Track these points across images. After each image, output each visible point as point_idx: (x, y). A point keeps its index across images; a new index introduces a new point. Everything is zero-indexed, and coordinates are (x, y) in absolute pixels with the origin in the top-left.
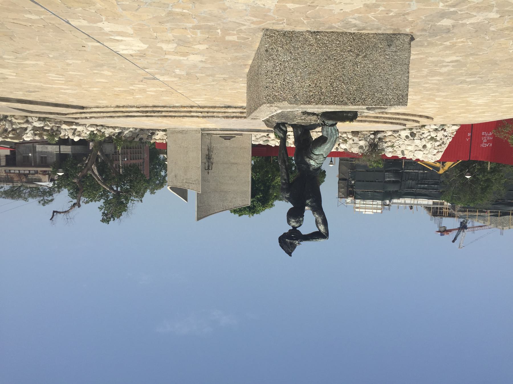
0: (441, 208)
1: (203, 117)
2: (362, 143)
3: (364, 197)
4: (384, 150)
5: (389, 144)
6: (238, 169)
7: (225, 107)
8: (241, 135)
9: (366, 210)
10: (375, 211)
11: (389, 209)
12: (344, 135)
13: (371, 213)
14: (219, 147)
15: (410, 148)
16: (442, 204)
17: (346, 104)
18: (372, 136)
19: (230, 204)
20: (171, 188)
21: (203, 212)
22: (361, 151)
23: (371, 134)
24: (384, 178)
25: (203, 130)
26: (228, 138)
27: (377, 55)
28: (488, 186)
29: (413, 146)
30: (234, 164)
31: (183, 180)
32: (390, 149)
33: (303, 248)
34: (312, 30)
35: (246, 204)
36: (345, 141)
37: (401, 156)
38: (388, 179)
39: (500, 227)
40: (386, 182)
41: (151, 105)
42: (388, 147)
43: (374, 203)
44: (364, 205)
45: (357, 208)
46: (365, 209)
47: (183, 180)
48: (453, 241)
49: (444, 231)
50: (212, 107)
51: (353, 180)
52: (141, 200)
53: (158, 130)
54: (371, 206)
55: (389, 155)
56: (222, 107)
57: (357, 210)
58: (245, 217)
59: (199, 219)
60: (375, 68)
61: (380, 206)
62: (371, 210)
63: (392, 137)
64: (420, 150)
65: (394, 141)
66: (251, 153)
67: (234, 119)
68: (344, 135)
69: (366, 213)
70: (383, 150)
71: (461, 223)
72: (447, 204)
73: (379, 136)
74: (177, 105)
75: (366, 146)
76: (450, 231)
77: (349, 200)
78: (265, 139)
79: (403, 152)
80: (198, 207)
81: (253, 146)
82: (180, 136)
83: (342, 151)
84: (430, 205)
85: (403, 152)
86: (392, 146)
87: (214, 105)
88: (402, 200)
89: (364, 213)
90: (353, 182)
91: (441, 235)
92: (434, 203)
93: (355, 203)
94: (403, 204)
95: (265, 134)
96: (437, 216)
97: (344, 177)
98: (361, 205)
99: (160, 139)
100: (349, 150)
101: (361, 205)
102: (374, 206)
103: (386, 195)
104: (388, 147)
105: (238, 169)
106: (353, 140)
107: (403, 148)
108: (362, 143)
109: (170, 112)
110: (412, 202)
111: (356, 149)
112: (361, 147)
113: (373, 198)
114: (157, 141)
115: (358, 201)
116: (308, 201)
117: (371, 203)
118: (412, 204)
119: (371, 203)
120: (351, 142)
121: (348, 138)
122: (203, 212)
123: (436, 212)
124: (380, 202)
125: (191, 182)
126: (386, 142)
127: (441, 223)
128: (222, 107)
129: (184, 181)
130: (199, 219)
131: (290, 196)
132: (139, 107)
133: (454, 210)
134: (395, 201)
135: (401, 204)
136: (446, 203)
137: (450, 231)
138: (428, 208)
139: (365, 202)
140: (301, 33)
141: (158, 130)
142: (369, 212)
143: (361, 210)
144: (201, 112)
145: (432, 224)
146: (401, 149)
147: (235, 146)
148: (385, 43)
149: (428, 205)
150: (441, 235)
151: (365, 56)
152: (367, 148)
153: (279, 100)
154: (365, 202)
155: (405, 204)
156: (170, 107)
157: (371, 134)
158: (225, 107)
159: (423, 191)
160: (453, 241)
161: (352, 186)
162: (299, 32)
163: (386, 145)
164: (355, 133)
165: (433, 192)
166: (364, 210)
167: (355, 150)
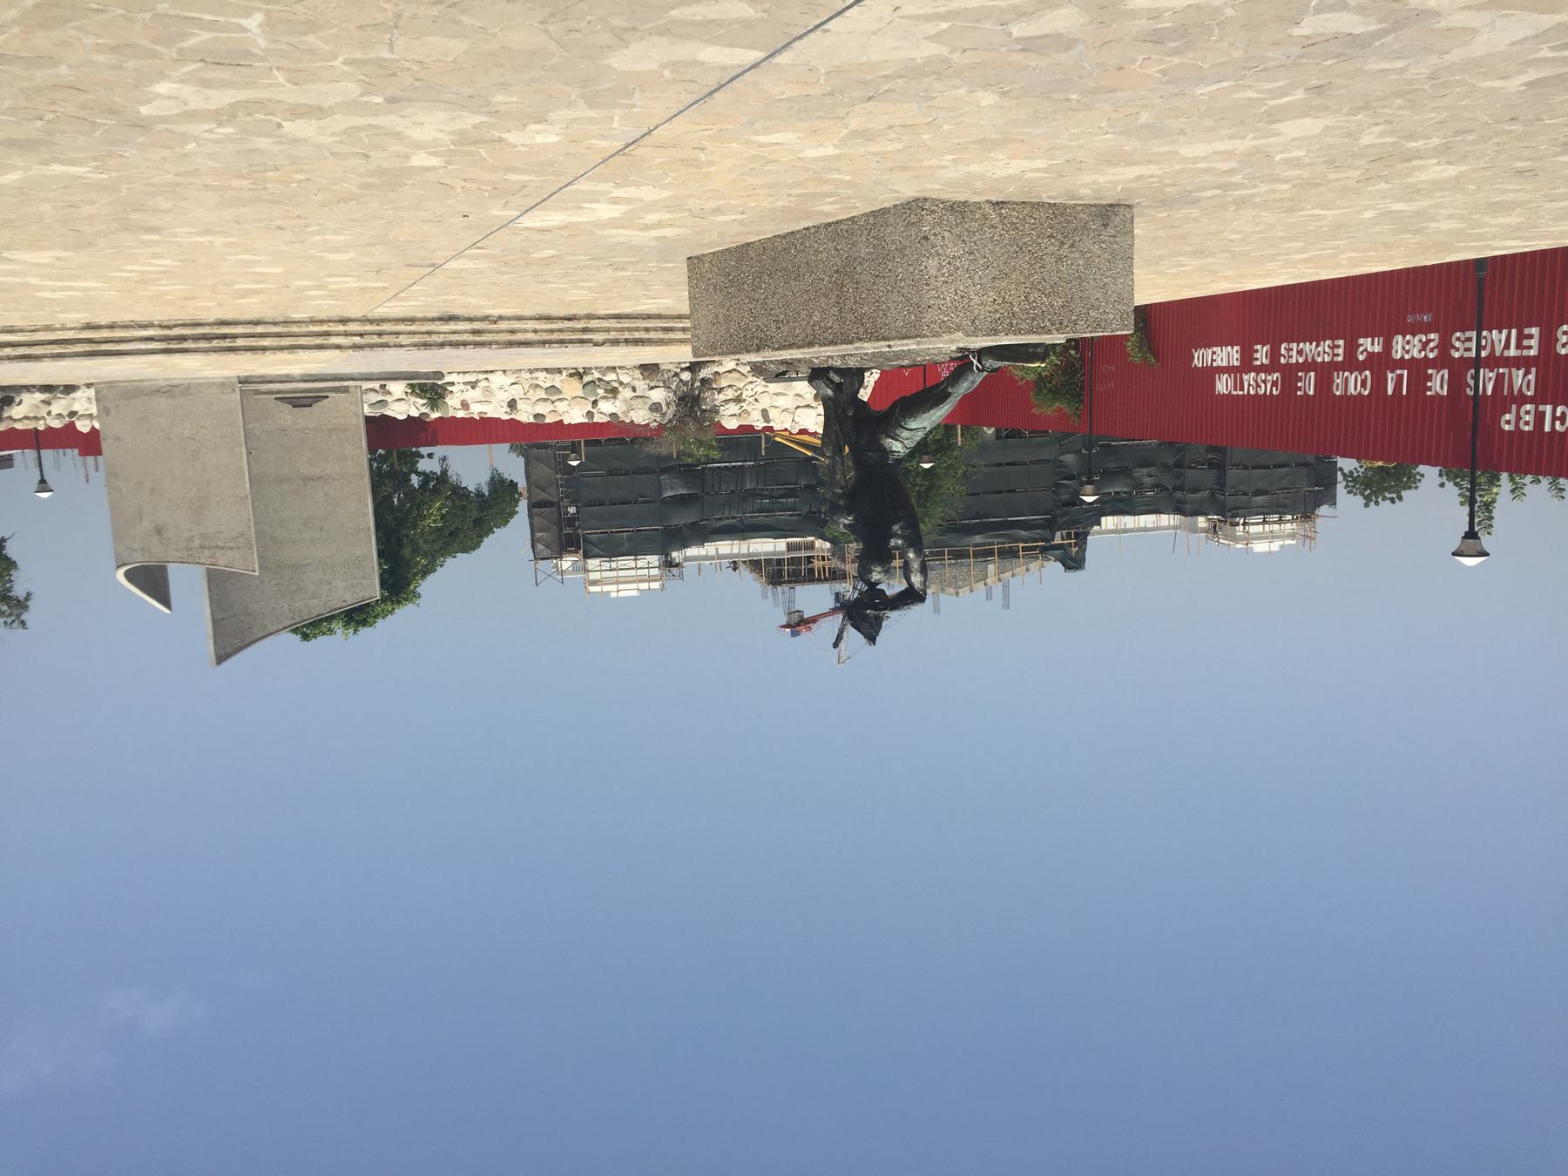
0: (809, 559)
1: (355, 347)
2: (659, 395)
3: (610, 550)
4: (717, 412)
5: (730, 394)
6: (326, 495)
7: (441, 319)
8: (346, 390)
9: (621, 587)
10: (644, 586)
11: (681, 577)
12: (611, 377)
13: (635, 593)
14: (257, 432)
15: (781, 402)
16: (811, 546)
17: (1049, 332)
18: (686, 376)
19: (315, 602)
20: (128, 575)
21: (231, 638)
22: (657, 416)
23: (683, 370)
24: (660, 490)
25: (244, 381)
26: (301, 401)
27: (1088, 243)
28: (930, 488)
29: (790, 397)
30: (307, 479)
31: (190, 539)
32: (733, 408)
33: (896, 623)
34: (994, 199)
35: (367, 595)
36: (613, 392)
37: (759, 424)
38: (669, 493)
39: (951, 590)
40: (664, 501)
41: (211, 320)
42: (727, 401)
43: (640, 563)
44: (614, 574)
45: (595, 583)
46: (617, 583)
47: (190, 539)
48: (836, 645)
49: (798, 623)
50: (403, 320)
51: (573, 503)
52: (23, 623)
53: (28, 388)
54: (632, 572)
55: (731, 424)
56: (433, 320)
57: (592, 589)
58: (338, 642)
59: (220, 659)
60: (1088, 266)
61: (655, 572)
62: (634, 586)
63: (734, 375)
64: (808, 406)
65: (740, 385)
66: (364, 444)
67: (447, 349)
68: (611, 377)
69: (621, 594)
70: (715, 410)
71: (837, 595)
72: (822, 546)
73: (704, 373)
74: (297, 316)
75: (668, 404)
76: (814, 620)
77: (567, 562)
78: (374, 398)
79: (765, 413)
80: (215, 622)
81: (369, 420)
82: (162, 403)
83: (605, 419)
84: (782, 553)
85: (765, 413)
86: (738, 400)
87: (410, 315)
88: (709, 548)
89: (614, 595)
90: (572, 510)
91: (794, 634)
92: (790, 547)
93: (586, 571)
94: (712, 558)
95: (376, 385)
96: (780, 584)
97: (543, 496)
98: (605, 574)
99: (27, 418)
100: (622, 417)
101: (605, 574)
102: (640, 572)
103: (666, 539)
104: (727, 401)
105: (326, 495)
106: (634, 389)
107: (765, 402)
108: (659, 395)
109: (262, 336)
110: (736, 551)
111: (642, 412)
112: (655, 407)
113: (635, 551)
114: (19, 426)
115: (593, 563)
116: (895, 528)
117: (632, 564)
118: (737, 555)
119: (632, 564)
120: (626, 393)
121: (621, 383)
122: (231, 638)
123: (776, 573)
124: (654, 560)
125: (220, 544)
126: (720, 390)
127: (791, 601)
128: (433, 320)
129: (196, 543)
130: (220, 659)
131: (855, 519)
132: (169, 327)
133: (843, 561)
134: (692, 551)
135: (706, 558)
136: (819, 543)
137: (814, 620)
138: (756, 565)
139: (614, 565)
140: (978, 205)
141: (28, 388)
142: (629, 591)
143: (606, 588)
144: (361, 335)
145: (765, 607)
146: (760, 406)
147: (311, 425)
148: (1099, 222)
149: (775, 553)
150: (794, 634)
151: (1072, 246)
152: (673, 408)
153: (949, 330)
154: (614, 565)
155: (720, 557)
156: (275, 324)
157: (683, 370)
158: (441, 319)
159: (761, 518)
160: (836, 645)
161: (571, 521)
162: (975, 204)
163: (721, 397)
164: (649, 370)
165: (783, 516)
166: (614, 587)
167: (641, 416)
